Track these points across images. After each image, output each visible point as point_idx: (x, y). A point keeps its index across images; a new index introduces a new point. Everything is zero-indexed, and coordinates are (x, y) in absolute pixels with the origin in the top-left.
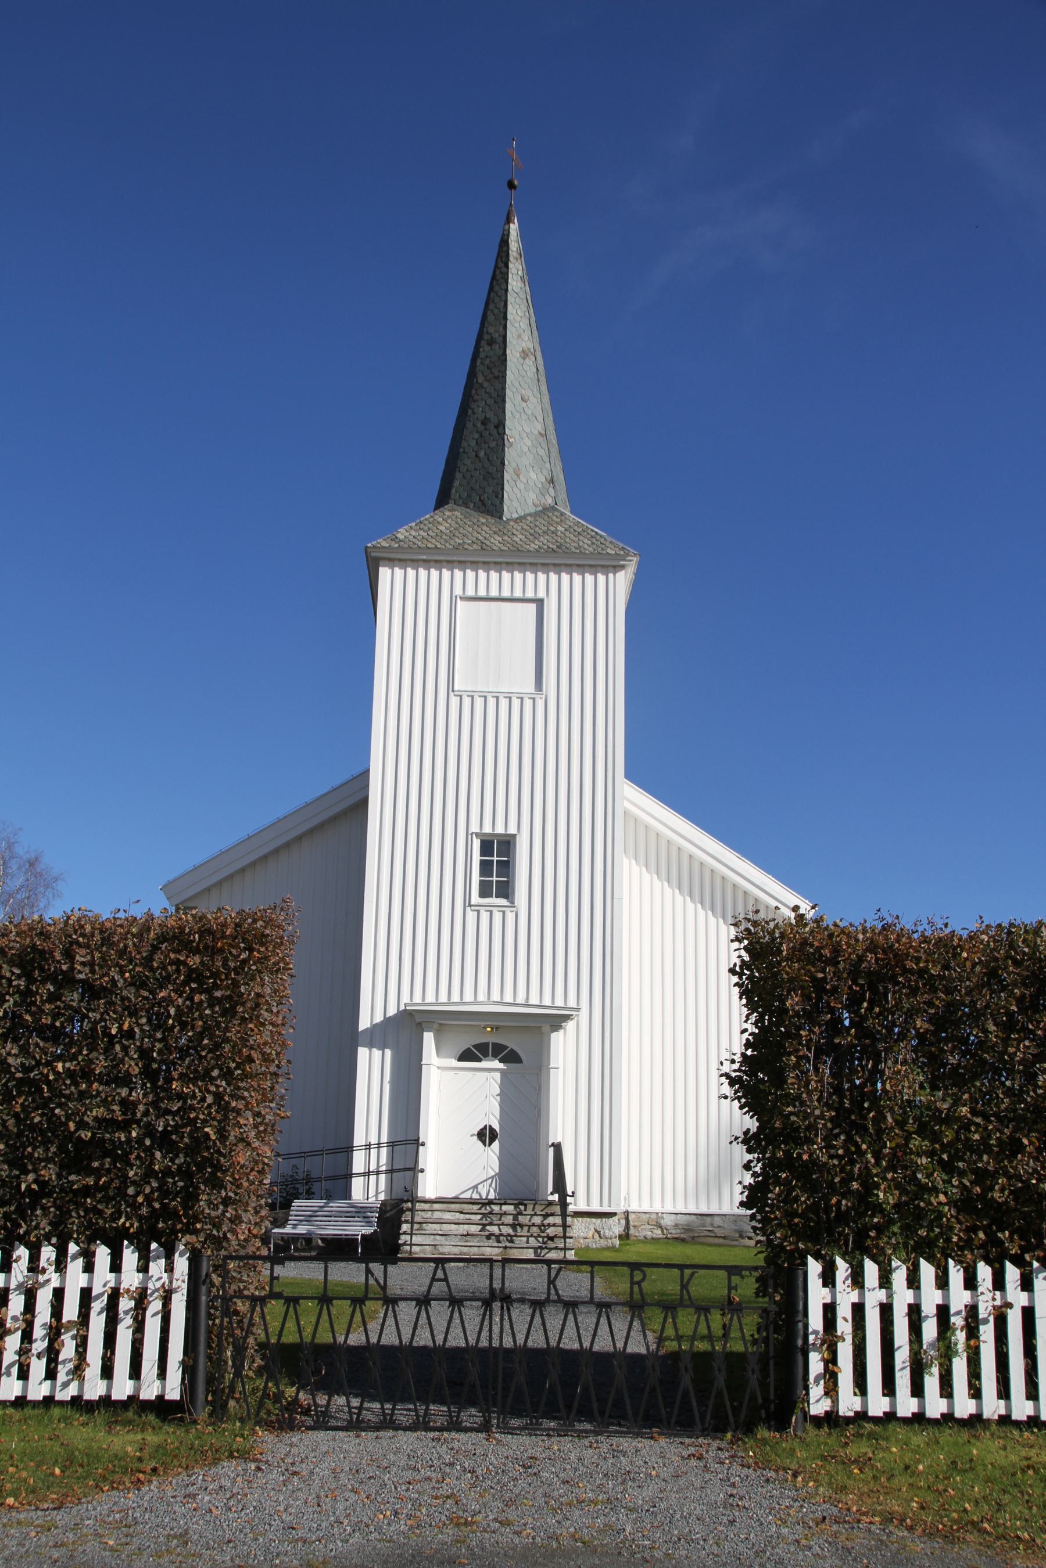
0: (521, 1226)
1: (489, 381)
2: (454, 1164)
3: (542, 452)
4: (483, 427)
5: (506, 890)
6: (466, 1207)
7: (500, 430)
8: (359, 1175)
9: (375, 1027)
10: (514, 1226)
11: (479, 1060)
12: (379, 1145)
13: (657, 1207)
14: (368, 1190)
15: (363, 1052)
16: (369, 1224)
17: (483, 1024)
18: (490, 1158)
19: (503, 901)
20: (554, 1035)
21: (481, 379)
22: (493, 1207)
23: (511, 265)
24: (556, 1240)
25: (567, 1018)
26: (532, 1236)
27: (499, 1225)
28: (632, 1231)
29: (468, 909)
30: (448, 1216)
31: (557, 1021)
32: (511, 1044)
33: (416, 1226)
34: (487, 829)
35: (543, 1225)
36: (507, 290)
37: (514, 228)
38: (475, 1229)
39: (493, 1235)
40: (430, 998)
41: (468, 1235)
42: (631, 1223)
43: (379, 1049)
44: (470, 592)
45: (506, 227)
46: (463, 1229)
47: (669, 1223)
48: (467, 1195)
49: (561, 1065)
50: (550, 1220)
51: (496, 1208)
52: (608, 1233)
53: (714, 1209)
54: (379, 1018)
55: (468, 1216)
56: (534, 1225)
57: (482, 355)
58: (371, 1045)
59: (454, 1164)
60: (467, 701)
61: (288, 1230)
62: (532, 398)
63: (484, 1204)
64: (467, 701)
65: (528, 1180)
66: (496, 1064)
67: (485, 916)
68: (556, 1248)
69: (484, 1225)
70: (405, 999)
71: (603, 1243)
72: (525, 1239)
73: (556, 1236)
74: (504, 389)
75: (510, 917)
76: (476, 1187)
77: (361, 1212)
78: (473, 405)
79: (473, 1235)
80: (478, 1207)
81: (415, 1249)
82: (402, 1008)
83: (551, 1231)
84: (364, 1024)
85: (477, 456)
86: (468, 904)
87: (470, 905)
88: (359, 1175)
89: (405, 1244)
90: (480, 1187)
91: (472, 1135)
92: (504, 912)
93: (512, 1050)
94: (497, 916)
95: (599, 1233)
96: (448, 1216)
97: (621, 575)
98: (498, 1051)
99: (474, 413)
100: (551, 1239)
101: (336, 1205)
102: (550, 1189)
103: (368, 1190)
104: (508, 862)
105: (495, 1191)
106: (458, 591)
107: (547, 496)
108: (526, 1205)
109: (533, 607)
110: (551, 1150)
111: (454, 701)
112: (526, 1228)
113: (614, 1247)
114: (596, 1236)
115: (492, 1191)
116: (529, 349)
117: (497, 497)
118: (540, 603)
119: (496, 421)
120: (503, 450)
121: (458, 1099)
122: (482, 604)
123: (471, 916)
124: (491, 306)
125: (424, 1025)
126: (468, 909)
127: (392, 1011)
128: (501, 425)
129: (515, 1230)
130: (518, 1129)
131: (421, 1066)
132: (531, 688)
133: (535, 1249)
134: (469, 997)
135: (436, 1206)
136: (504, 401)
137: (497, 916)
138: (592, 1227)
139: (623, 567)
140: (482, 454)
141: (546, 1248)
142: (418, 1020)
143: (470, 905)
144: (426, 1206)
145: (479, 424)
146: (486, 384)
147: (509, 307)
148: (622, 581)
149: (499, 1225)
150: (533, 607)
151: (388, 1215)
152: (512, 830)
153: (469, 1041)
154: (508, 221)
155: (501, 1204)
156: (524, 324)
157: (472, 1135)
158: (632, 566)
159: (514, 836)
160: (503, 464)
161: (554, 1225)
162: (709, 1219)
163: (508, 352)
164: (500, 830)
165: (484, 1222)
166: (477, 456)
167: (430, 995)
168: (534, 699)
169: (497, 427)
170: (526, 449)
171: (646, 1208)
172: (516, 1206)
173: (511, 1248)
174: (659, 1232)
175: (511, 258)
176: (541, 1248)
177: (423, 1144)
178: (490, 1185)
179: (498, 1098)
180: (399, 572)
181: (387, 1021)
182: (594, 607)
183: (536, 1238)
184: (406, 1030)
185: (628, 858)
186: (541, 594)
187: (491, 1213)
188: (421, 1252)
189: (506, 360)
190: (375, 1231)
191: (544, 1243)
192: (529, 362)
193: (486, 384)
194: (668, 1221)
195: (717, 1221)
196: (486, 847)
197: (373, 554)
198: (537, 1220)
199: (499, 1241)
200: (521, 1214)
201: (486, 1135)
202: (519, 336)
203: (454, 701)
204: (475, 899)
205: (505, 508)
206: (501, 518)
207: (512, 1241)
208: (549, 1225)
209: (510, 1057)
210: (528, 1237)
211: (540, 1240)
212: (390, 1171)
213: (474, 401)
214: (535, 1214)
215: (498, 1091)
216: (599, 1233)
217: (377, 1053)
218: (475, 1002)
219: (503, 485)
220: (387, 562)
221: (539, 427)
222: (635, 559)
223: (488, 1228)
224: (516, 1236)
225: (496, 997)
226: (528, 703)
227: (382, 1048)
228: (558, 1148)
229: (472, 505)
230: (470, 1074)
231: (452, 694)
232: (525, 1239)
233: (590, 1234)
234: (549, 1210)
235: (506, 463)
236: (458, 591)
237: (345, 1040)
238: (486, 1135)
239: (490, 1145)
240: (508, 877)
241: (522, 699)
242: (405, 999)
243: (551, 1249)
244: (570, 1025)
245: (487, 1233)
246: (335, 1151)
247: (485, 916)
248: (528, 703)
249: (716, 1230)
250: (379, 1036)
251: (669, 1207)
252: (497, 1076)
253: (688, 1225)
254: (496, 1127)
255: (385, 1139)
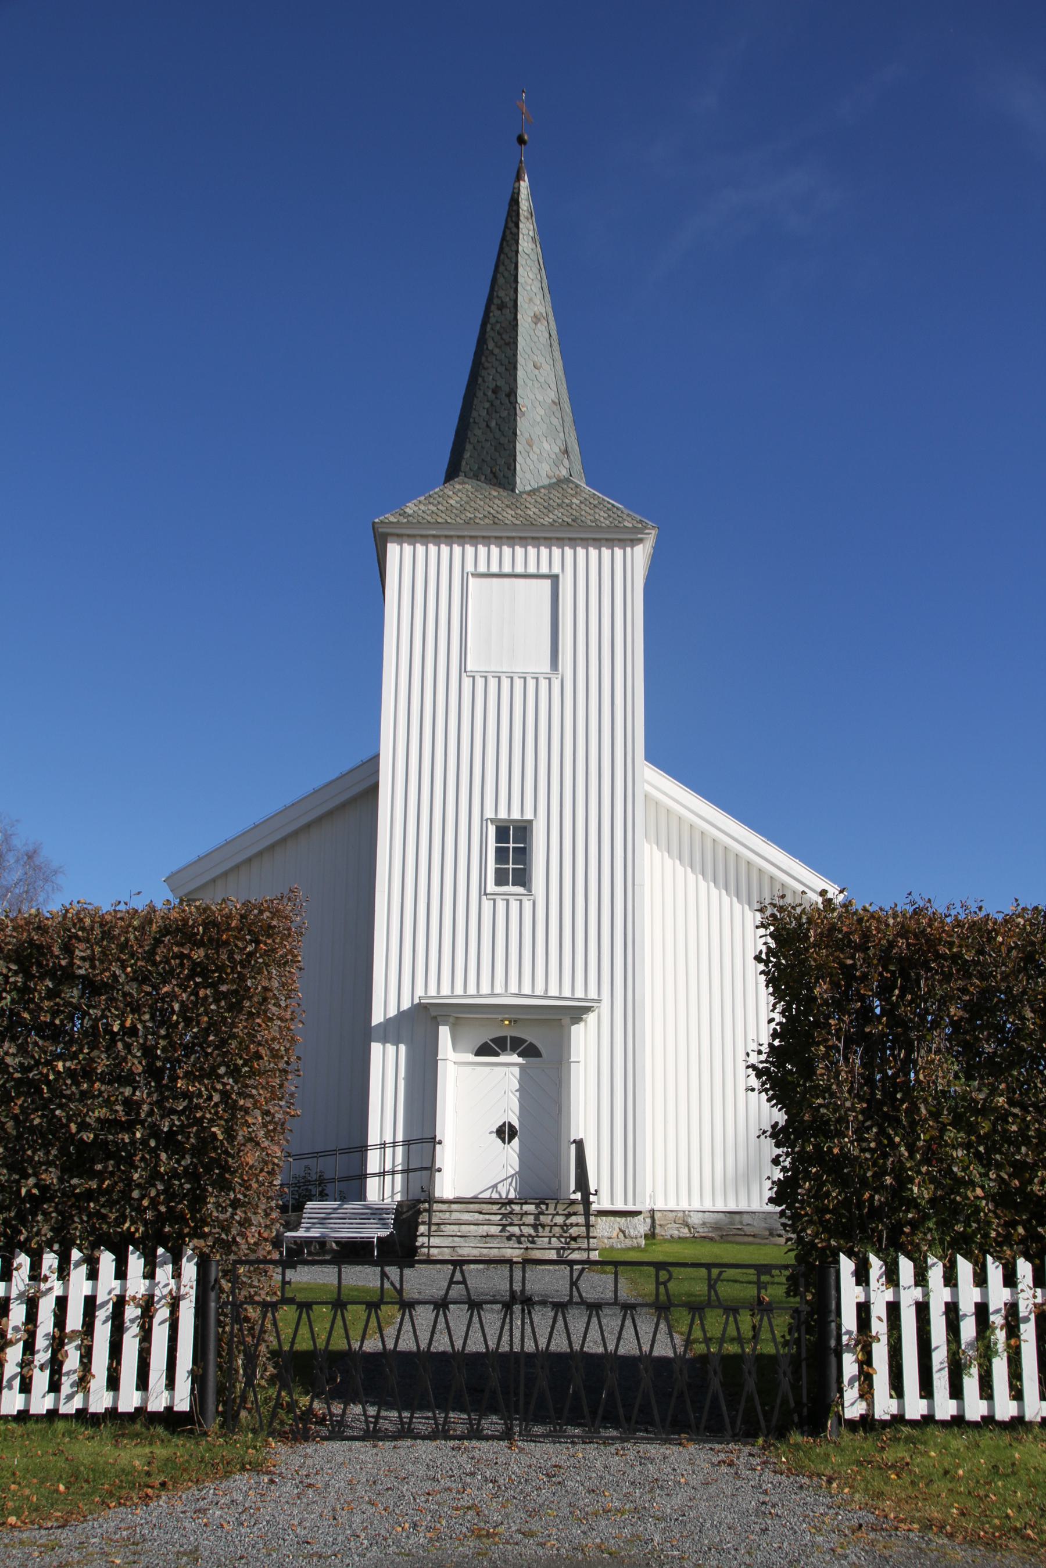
0: (543, 1226)
1: (500, 347)
2: (472, 1162)
3: (555, 422)
4: (494, 396)
5: (522, 878)
6: (486, 1207)
7: (512, 399)
8: (374, 1175)
9: (388, 1021)
10: (535, 1227)
11: (497, 1055)
12: (394, 1144)
13: (684, 1206)
14: (384, 1190)
15: (376, 1048)
16: (385, 1226)
17: (500, 1017)
18: (507, 1158)
19: (520, 890)
20: (574, 1028)
21: (491, 345)
22: (513, 1206)
23: (521, 225)
24: (579, 1240)
25: (587, 1010)
26: (554, 1236)
27: (519, 1225)
28: (658, 1230)
29: (484, 898)
30: (466, 1217)
31: (577, 1013)
32: (530, 1037)
33: (433, 1228)
34: (503, 815)
35: (565, 1225)
36: (517, 252)
37: (524, 185)
38: (495, 1230)
39: (514, 1235)
40: (446, 991)
41: (488, 1236)
42: (657, 1222)
43: (393, 1044)
44: (482, 568)
45: (516, 185)
46: (483, 1230)
47: (697, 1221)
48: (486, 1195)
49: (582, 1059)
50: (573, 1219)
51: (517, 1208)
52: (633, 1233)
53: (743, 1207)
54: (392, 1012)
55: (487, 1217)
56: (556, 1225)
57: (492, 320)
58: (384, 1041)
59: (472, 1162)
60: (480, 682)
61: (301, 1233)
62: (545, 366)
63: (504, 1204)
64: (480, 682)
65: (550, 1179)
66: (515, 1058)
67: (501, 905)
68: (579, 1249)
69: (504, 1226)
70: (420, 992)
71: (628, 1243)
72: (546, 1240)
73: (579, 1236)
74: (515, 355)
75: (527, 905)
76: (495, 1186)
77: (376, 1213)
78: (484, 373)
79: (492, 1236)
80: (498, 1206)
81: (433, 1251)
82: (416, 1001)
83: (574, 1231)
84: (377, 1018)
85: (488, 426)
86: (483, 893)
87: (486, 894)
88: (374, 1175)
89: (422, 1246)
90: (500, 1186)
91: (491, 1133)
92: (521, 901)
93: (531, 1044)
94: (514, 905)
95: (623, 1232)
96: (466, 1217)
97: (639, 549)
98: (517, 1045)
99: (484, 381)
100: (574, 1239)
101: (351, 1206)
102: (573, 1187)
103: (384, 1190)
104: (524, 848)
105: (515, 1190)
106: (470, 568)
107: (561, 468)
108: (547, 1204)
109: (548, 583)
110: (573, 1147)
111: (467, 682)
112: (547, 1229)
113: (639, 1247)
114: (621, 1235)
115: (512, 1190)
116: (541, 314)
117: (509, 469)
118: (554, 579)
119: (508, 390)
120: (515, 420)
121: (476, 1094)
122: (495, 580)
123: (487, 904)
124: (501, 268)
125: (439, 1019)
126: (484, 898)
127: (406, 1005)
128: (512, 394)
129: (536, 1230)
130: (539, 1127)
131: (437, 1061)
132: (546, 667)
133: (558, 1250)
134: (485, 989)
135: (454, 1207)
136: (515, 368)
137: (514, 905)
138: (616, 1226)
139: (641, 541)
140: (493, 424)
141: (569, 1248)
142: (433, 1014)
143: (486, 894)
144: (444, 1207)
145: (490, 393)
146: (496, 351)
147: (520, 270)
148: (640, 555)
149: (519, 1225)
150: (548, 583)
151: (404, 1216)
152: (529, 815)
153: (486, 1036)
154: (519, 178)
155: (522, 1204)
156: (536, 287)
157: (491, 1133)
158: (650, 538)
159: (530, 822)
160: (516, 434)
161: (577, 1225)
162: (737, 1217)
163: (519, 317)
164: (516, 815)
165: (504, 1222)
166: (488, 426)
167: (446, 989)
168: (549, 679)
169: (508, 395)
170: (539, 419)
171: (672, 1206)
172: (537, 1205)
173: (532, 1249)
174: (686, 1230)
175: (522, 218)
176: (563, 1248)
177: (440, 1143)
178: (510, 1184)
179: (517, 1094)
180: (407, 548)
181: (401, 1015)
182: (610, 582)
183: (558, 1238)
184: (421, 1024)
185: (650, 843)
186: (556, 569)
187: (511, 1213)
188: (439, 1254)
189: (517, 325)
190: (391, 1233)
191: (567, 1243)
192: (542, 327)
193: (496, 351)
194: (695, 1220)
195: (746, 1219)
196: (502, 833)
197: (380, 530)
198: (559, 1220)
199: (520, 1242)
200: (543, 1214)
201: (506, 1133)
202: (531, 300)
203: (467, 682)
204: (491, 887)
205: (518, 480)
206: (513, 490)
207: (533, 1242)
208: (572, 1225)
209: (530, 1051)
210: (550, 1237)
211: (563, 1240)
212: (406, 1171)
213: (485, 369)
214: (557, 1214)
215: (517, 1087)
216: (623, 1232)
217: (391, 1048)
218: (493, 995)
219: (515, 456)
220: (395, 538)
221: (552, 395)
222: (653, 532)
223: (508, 1228)
224: (537, 1236)
225: (513, 988)
226: (544, 684)
227: (396, 1043)
228: (580, 1144)
229: (483, 478)
230: (488, 1069)
231: (464, 675)
232: (546, 1240)
233: (615, 1234)
234: (571, 1210)
235: (518, 433)
236: (470, 568)
237: (358, 1035)
238: (506, 1133)
239: (509, 1142)
240: (525, 864)
241: (537, 679)
242: (420, 992)
243: (574, 1250)
244: (591, 1018)
245: (507, 1234)
246: (348, 1151)
247: (501, 905)
248: (544, 684)
249: (745, 1228)
250: (393, 1031)
251: (696, 1205)
252: (516, 1070)
253: (716, 1223)
254: (516, 1124)
255: (400, 1137)
